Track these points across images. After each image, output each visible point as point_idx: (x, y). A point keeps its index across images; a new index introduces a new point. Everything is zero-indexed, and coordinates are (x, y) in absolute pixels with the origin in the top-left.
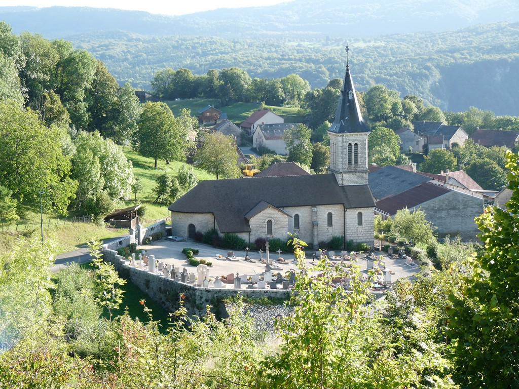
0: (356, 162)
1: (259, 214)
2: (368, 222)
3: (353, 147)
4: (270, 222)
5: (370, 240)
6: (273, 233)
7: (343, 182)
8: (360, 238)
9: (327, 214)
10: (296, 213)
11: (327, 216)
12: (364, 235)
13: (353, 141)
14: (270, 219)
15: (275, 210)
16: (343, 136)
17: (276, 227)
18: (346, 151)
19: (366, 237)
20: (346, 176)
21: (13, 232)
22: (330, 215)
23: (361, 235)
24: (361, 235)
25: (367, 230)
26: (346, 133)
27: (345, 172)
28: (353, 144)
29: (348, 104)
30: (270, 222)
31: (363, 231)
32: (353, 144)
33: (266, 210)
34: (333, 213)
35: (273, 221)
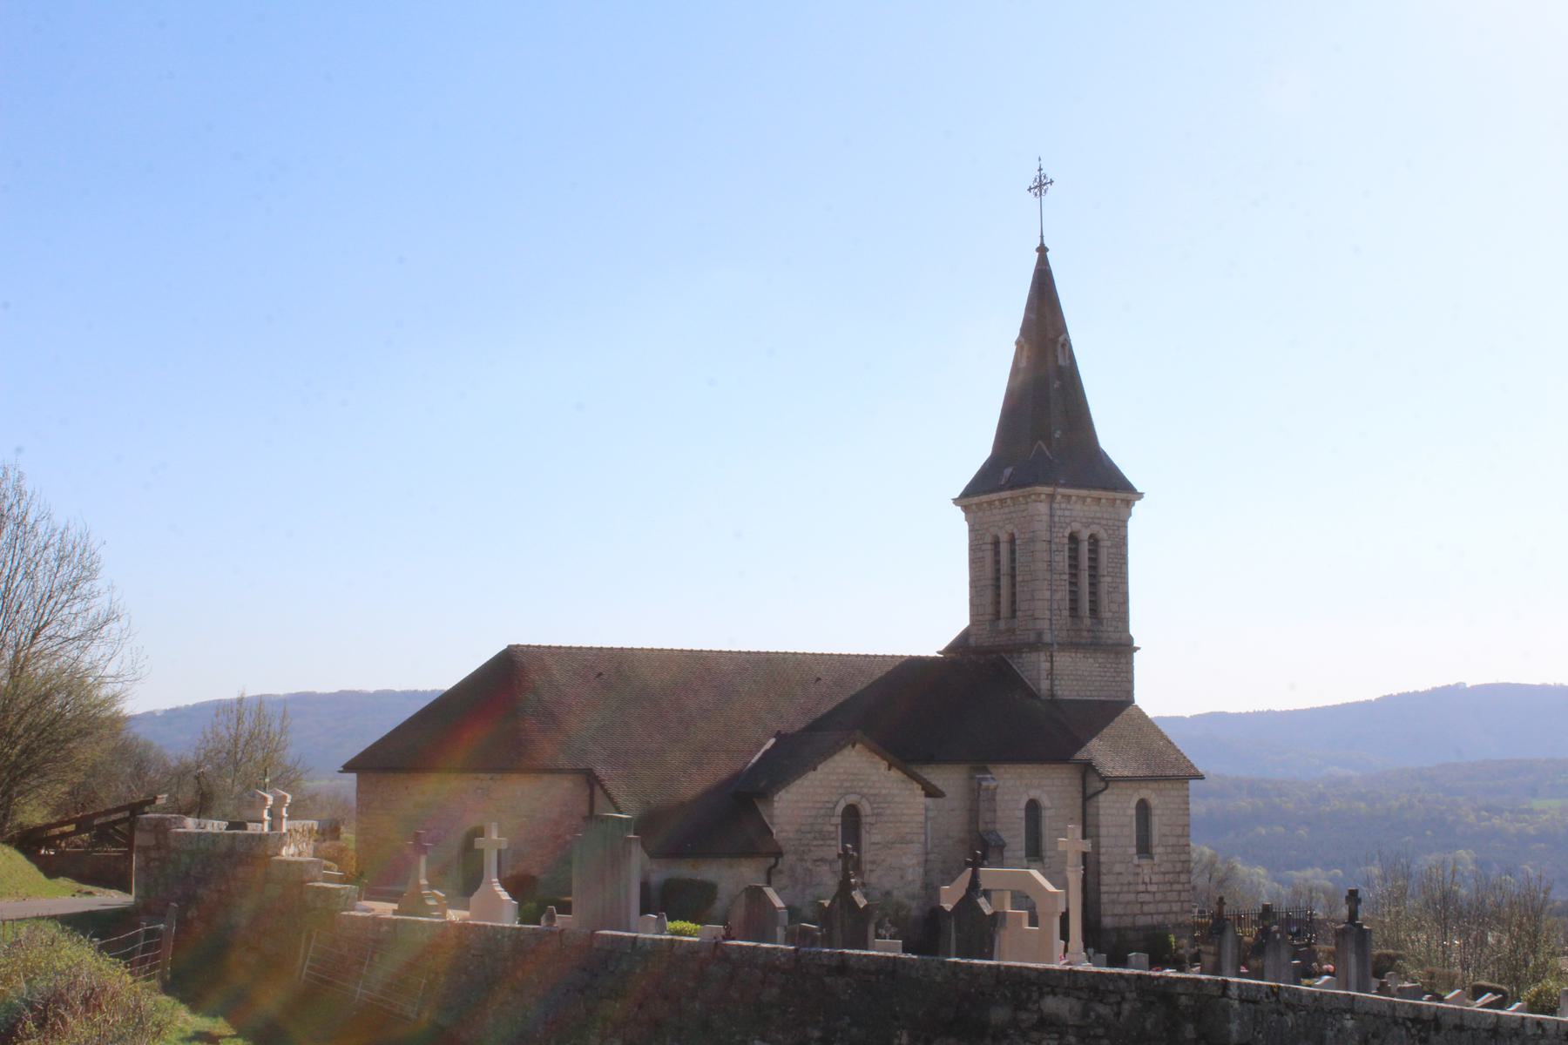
0: (1094, 611)
1: (811, 775)
2: (1172, 841)
3: (1084, 548)
4: (852, 817)
5: (1181, 919)
6: (866, 867)
7: (1052, 685)
8: (1146, 908)
9: (1023, 804)
10: (1034, 794)
11: (1022, 814)
12: (1159, 897)
13: (1087, 526)
14: (852, 799)
15: (877, 759)
16: (1052, 497)
17: (877, 838)
18: (1062, 561)
19: (1164, 907)
20: (1064, 660)
21: (189, 914)
22: (1033, 808)
23: (1148, 897)
24: (1148, 897)
25: (1168, 877)
26: (1064, 486)
27: (1063, 646)
28: (1004, 537)
29: (1057, 384)
30: (852, 817)
31: (1155, 878)
32: (1004, 537)
33: (837, 757)
34: (1045, 801)
35: (865, 808)
